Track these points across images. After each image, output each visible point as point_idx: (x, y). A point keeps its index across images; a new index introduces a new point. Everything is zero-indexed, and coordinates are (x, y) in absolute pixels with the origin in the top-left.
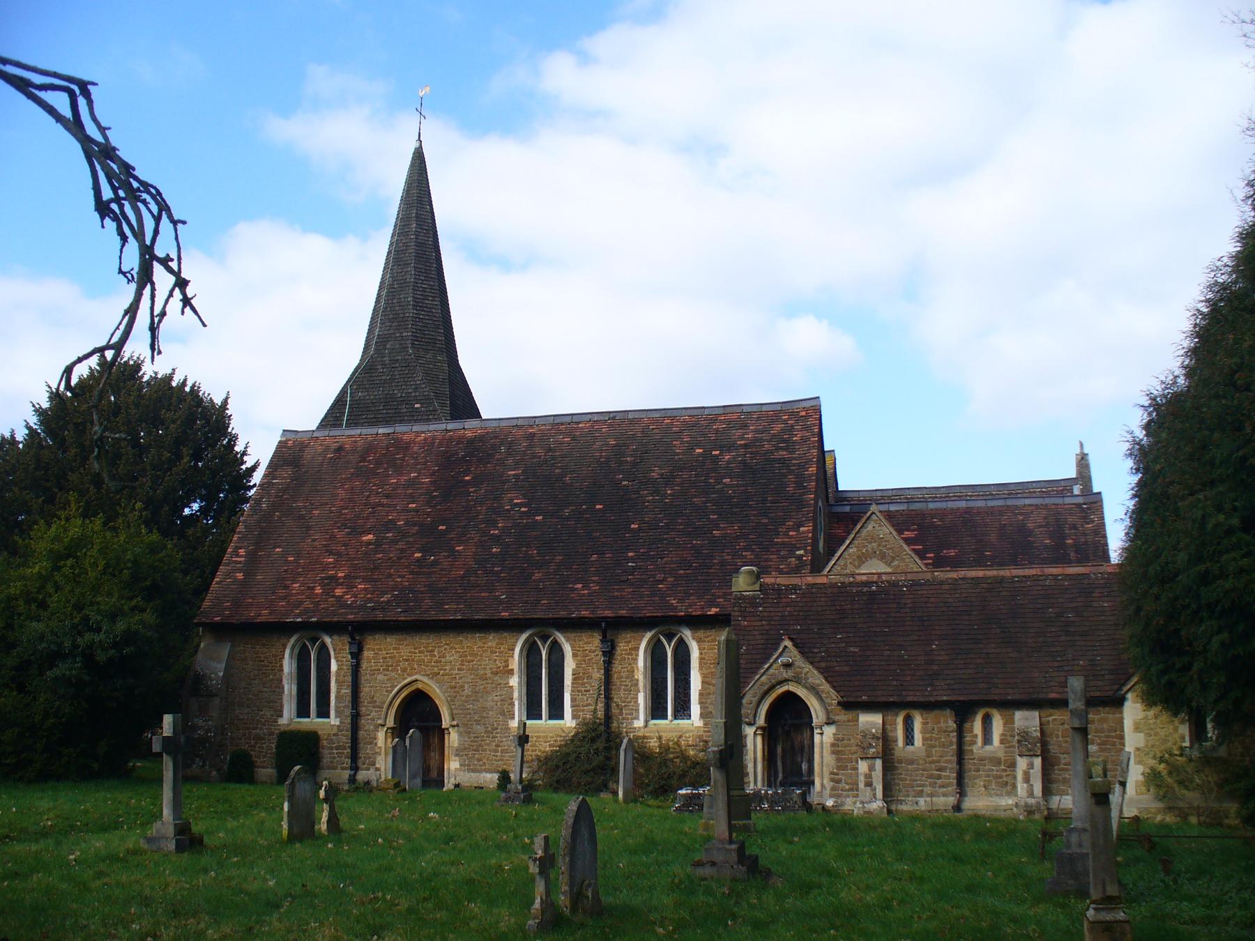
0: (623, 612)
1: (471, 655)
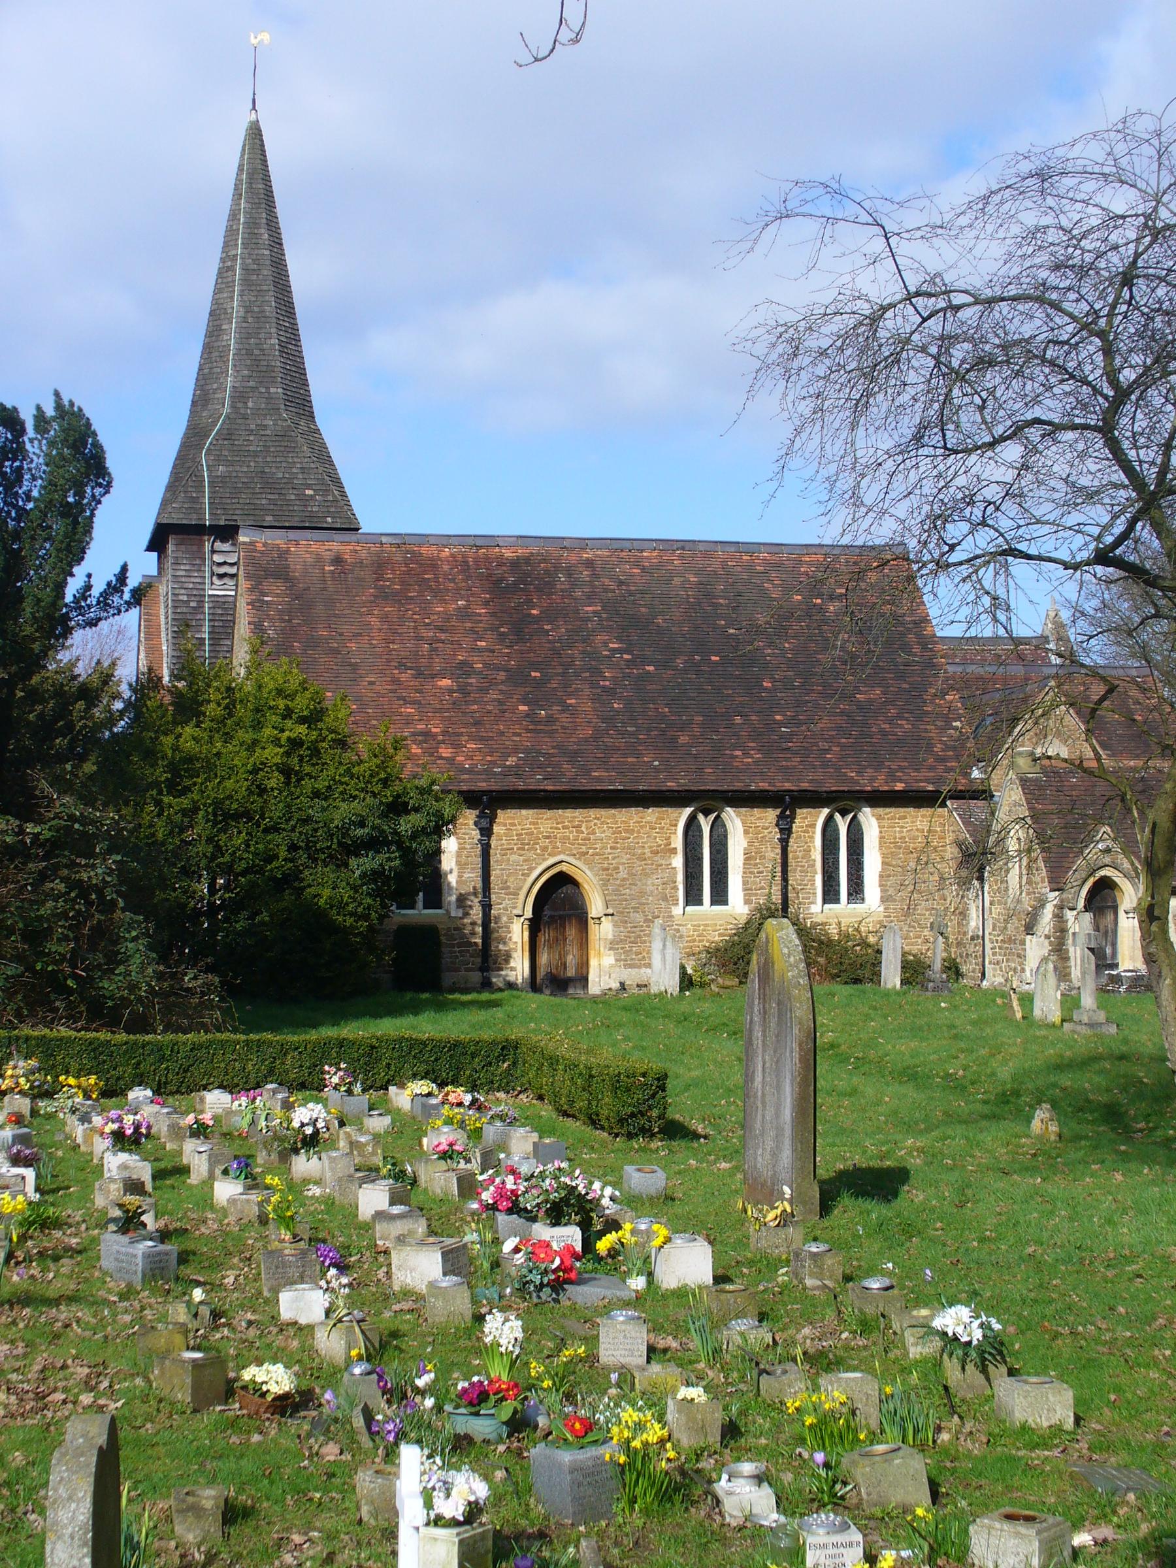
0: (805, 786)
1: (626, 831)
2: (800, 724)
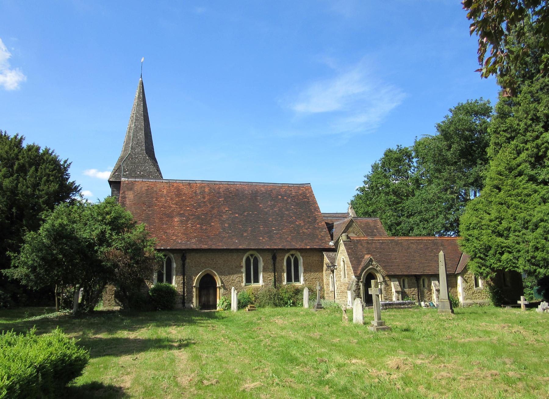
0: (280, 247)
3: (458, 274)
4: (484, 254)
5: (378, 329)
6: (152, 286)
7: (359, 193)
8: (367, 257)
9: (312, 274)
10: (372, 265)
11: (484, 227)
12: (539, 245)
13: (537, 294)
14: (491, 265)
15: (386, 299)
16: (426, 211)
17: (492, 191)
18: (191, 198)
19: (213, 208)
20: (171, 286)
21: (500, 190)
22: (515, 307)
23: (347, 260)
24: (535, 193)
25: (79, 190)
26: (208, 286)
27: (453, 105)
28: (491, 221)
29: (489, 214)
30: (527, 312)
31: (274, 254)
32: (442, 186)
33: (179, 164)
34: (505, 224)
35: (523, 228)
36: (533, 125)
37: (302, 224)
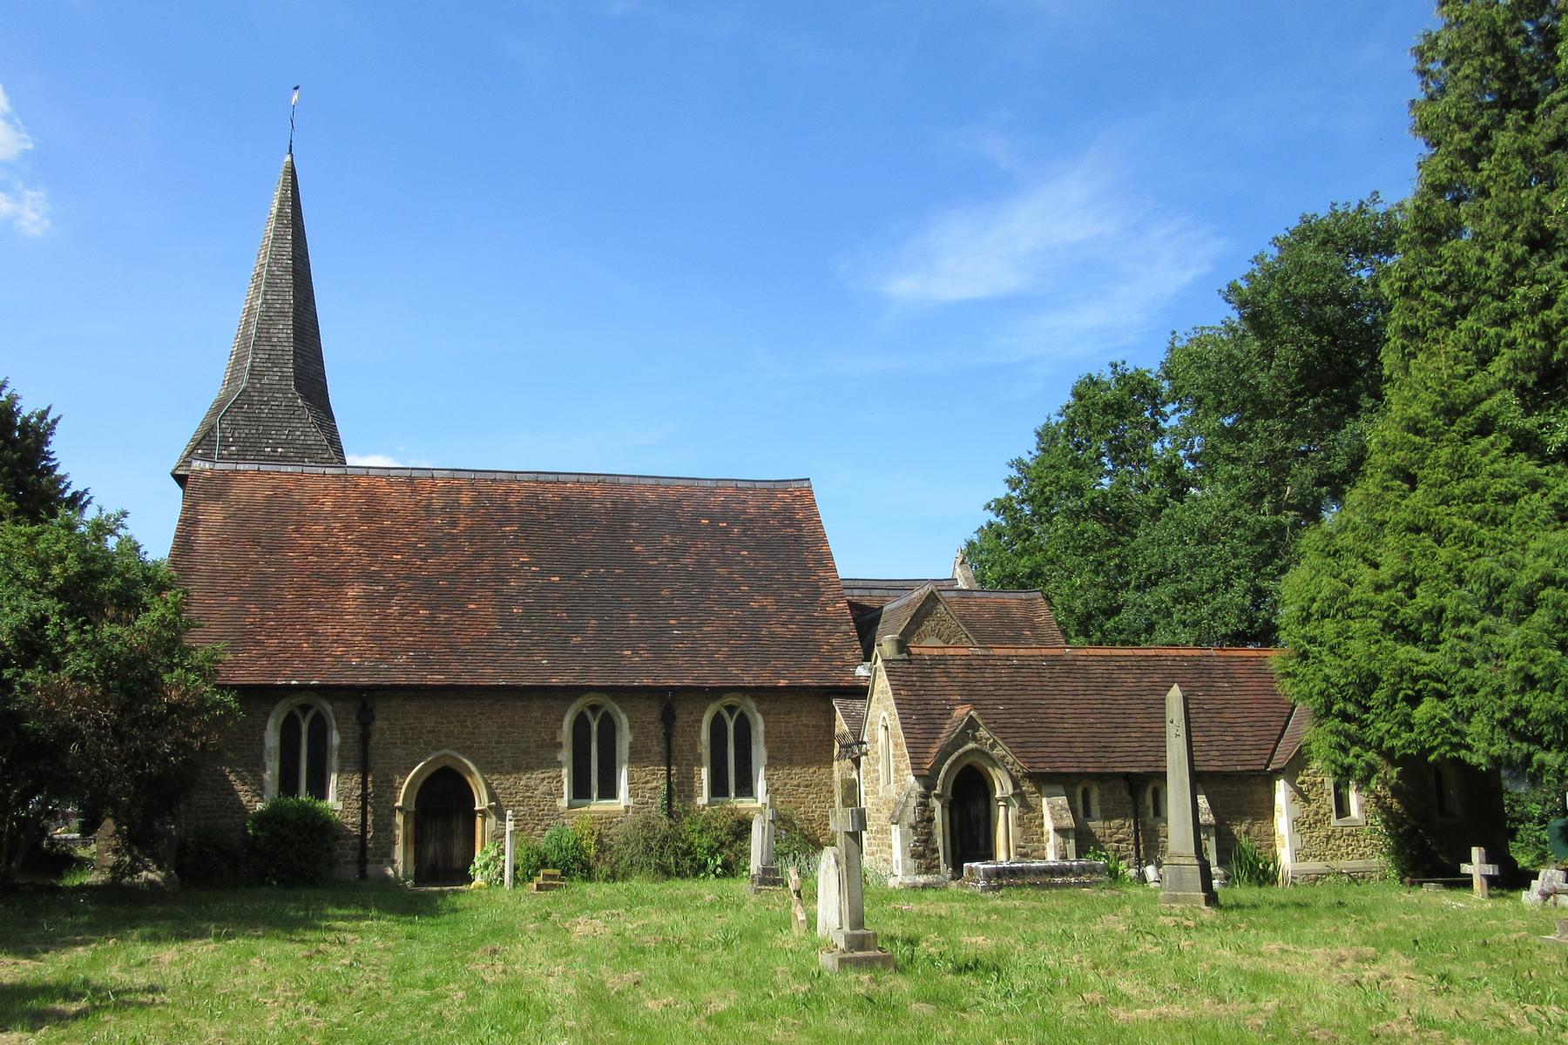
0: (687, 682)
2: (690, 628)
3: (1278, 773)
4: (1358, 703)
5: (842, 962)
6: (259, 806)
7: (994, 519)
8: (961, 712)
9: (796, 770)
10: (975, 739)
11: (1357, 610)
12: (1537, 670)
13: (1560, 844)
14: (1381, 740)
15: (1025, 855)
16: (1191, 567)
17: (1387, 488)
18: (409, 524)
19: (479, 555)
20: (320, 805)
21: (1412, 481)
22: (1450, 885)
23: (895, 723)
24: (1534, 490)
25: (84, 506)
26: (445, 811)
27: (1286, 222)
28: (1379, 588)
29: (1376, 566)
30: (1489, 905)
31: (669, 705)
32: (1244, 486)
33: (396, 423)
34: (1424, 598)
35: (1484, 610)
36: (1533, 264)
37: (771, 609)
